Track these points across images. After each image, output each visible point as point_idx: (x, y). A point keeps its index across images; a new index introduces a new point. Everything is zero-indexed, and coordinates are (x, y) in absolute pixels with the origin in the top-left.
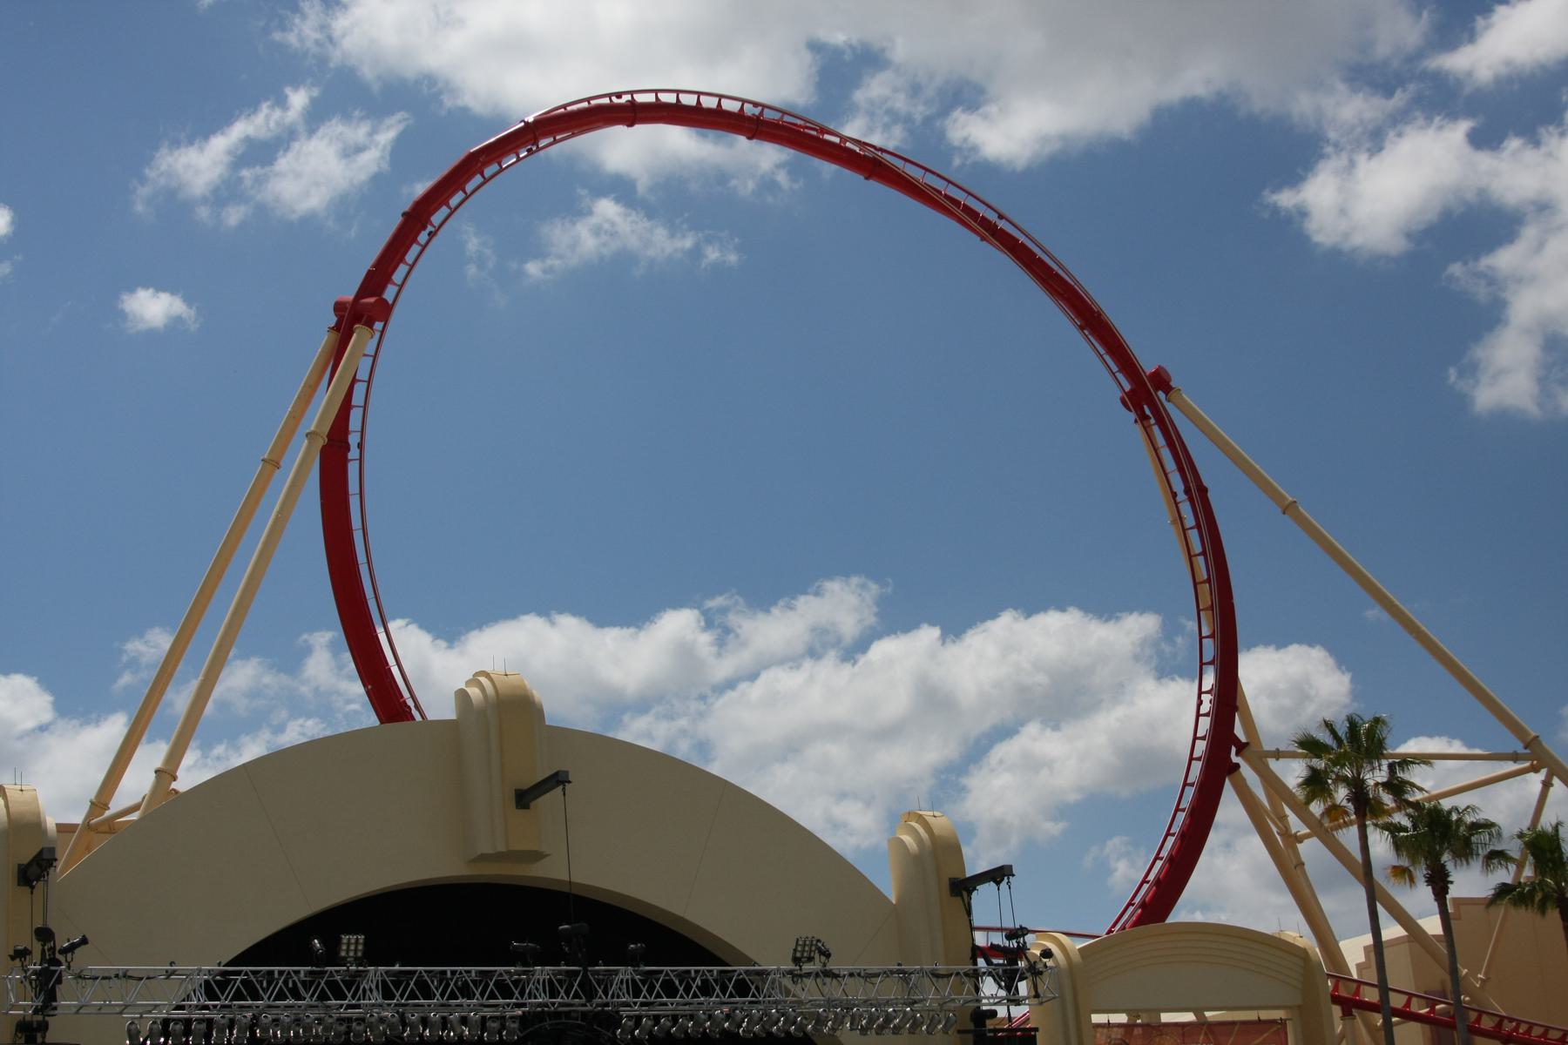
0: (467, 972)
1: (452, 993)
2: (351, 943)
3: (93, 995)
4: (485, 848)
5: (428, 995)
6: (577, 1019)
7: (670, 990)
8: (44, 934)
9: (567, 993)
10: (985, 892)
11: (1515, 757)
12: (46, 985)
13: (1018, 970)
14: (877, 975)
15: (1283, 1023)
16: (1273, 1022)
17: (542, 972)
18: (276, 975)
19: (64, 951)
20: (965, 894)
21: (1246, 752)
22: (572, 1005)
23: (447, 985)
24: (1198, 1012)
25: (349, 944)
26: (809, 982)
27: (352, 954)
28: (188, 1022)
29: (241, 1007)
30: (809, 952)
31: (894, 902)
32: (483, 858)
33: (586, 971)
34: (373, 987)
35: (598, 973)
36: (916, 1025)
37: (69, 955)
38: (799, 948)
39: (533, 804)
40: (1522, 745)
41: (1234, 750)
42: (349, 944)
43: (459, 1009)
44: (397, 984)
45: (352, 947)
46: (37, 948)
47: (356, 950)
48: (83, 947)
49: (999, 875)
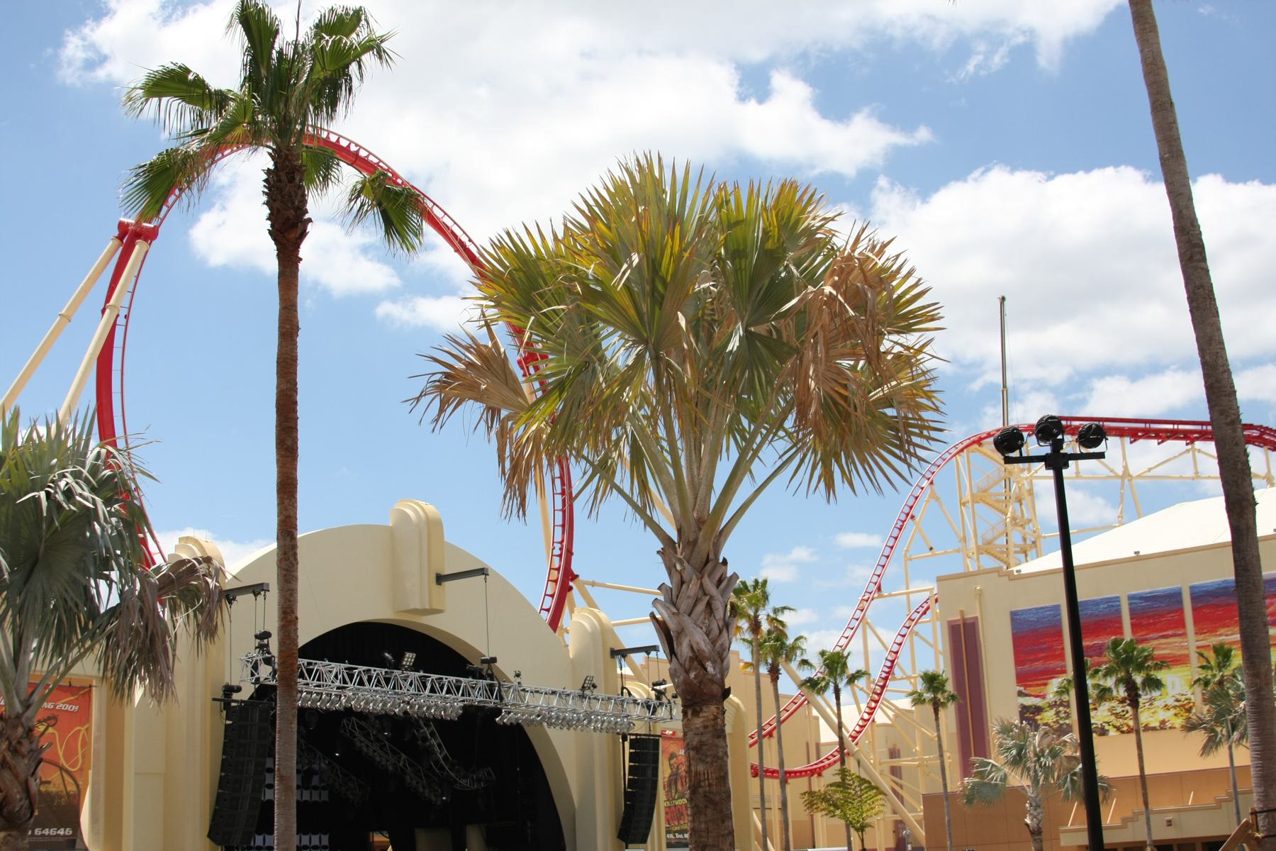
39: (443, 584)
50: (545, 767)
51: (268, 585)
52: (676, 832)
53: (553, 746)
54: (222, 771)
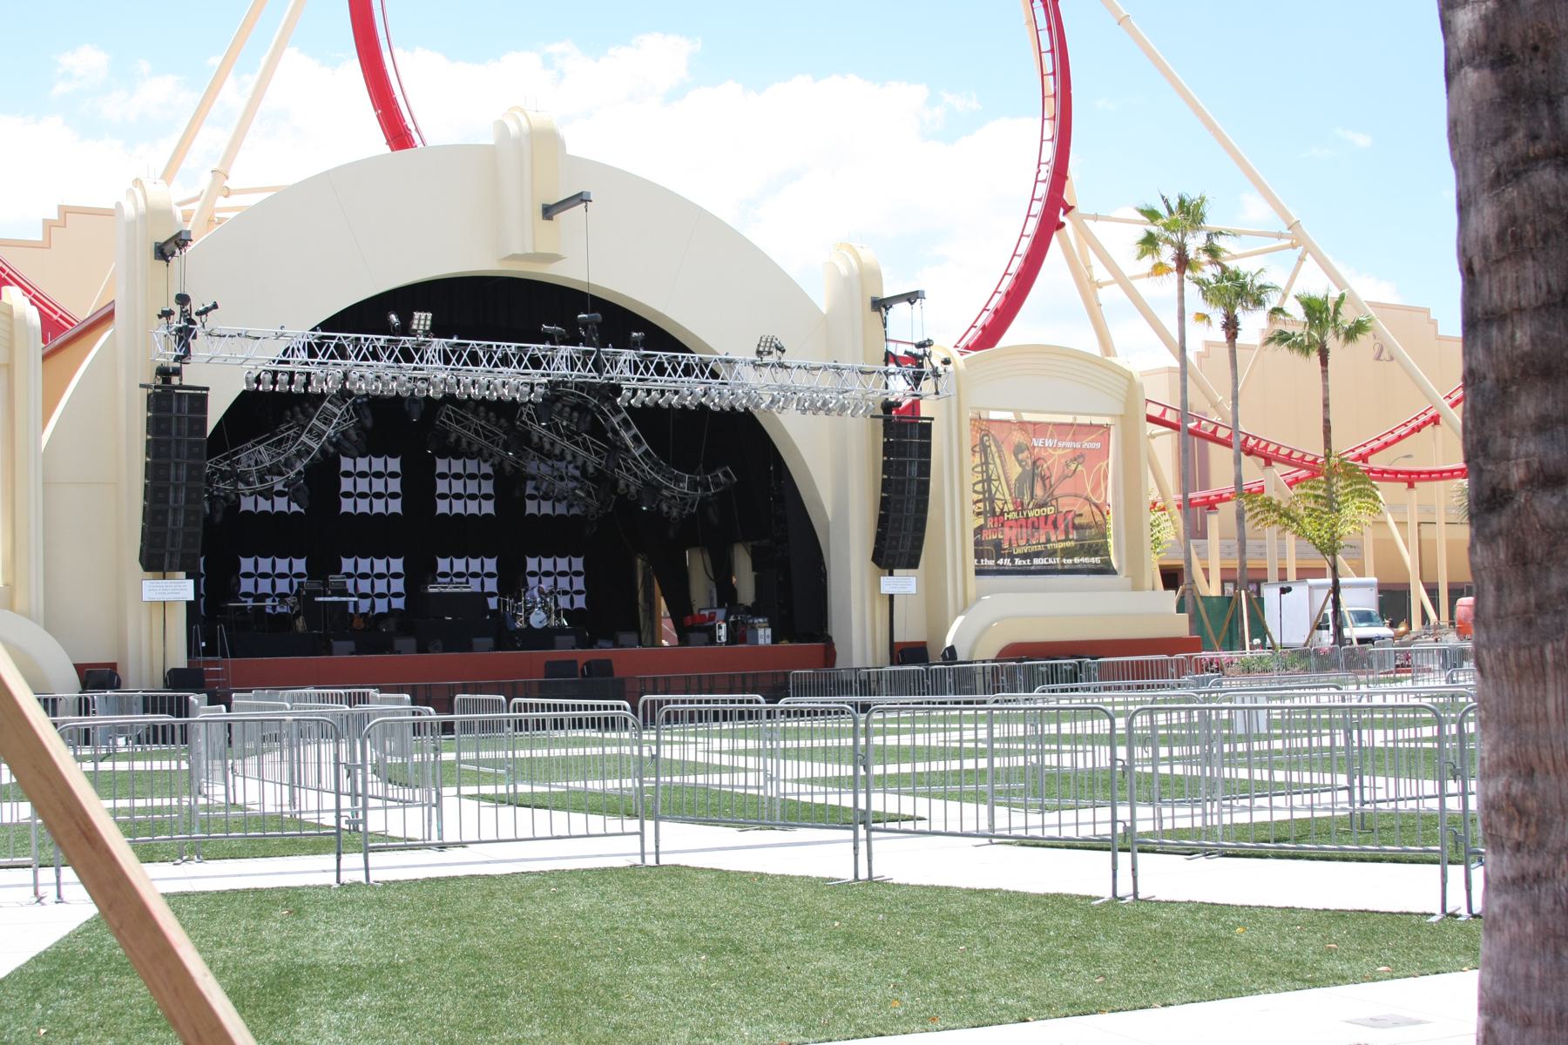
0: (509, 347)
1: (365, 356)
2: (422, 320)
3: (219, 347)
4: (517, 250)
5: (344, 356)
6: (571, 388)
7: (660, 370)
8: (183, 299)
9: (584, 368)
10: (899, 311)
11: (1280, 236)
12: (185, 335)
13: (923, 373)
14: (819, 369)
15: (1108, 427)
16: (1101, 426)
17: (565, 350)
18: (495, 348)
19: (199, 314)
20: (883, 310)
21: (1071, 213)
22: (586, 377)
23: (361, 349)
24: (1017, 412)
25: (419, 320)
26: (766, 371)
27: (421, 327)
28: (292, 374)
29: (335, 364)
30: (768, 352)
31: (825, 312)
32: (514, 257)
33: (599, 351)
34: (301, 348)
35: (606, 353)
36: (843, 408)
37: (204, 317)
38: (762, 344)
39: (555, 217)
40: (1286, 227)
41: (1062, 210)
42: (419, 320)
43: (501, 375)
44: (453, 352)
45: (422, 322)
46: (177, 309)
47: (425, 325)
48: (214, 311)
49: (912, 297)
50: (788, 464)
51: (923, 292)
52: (1017, 556)
53: (789, 436)
54: (883, 491)
